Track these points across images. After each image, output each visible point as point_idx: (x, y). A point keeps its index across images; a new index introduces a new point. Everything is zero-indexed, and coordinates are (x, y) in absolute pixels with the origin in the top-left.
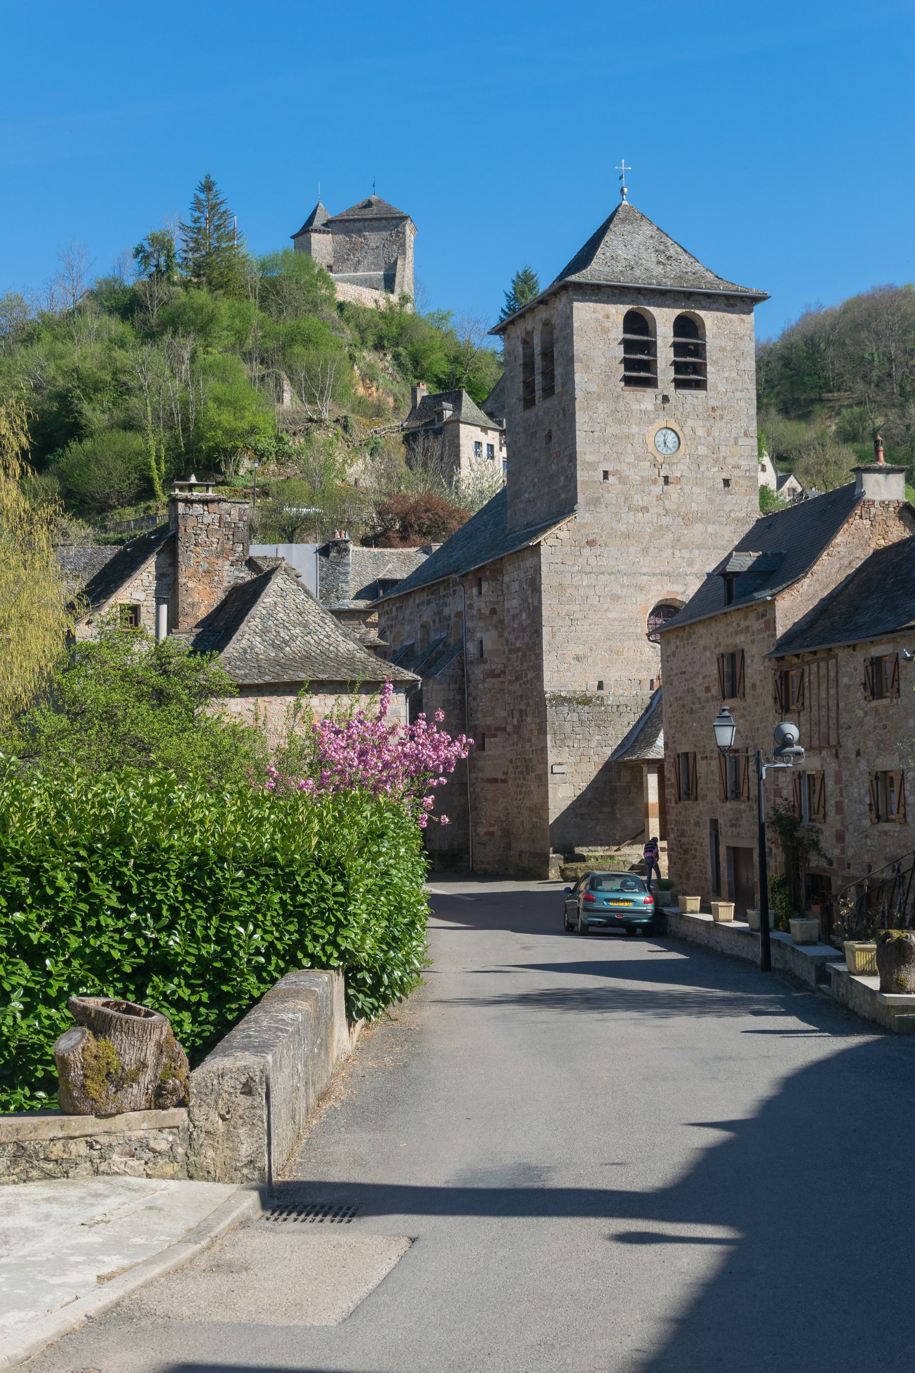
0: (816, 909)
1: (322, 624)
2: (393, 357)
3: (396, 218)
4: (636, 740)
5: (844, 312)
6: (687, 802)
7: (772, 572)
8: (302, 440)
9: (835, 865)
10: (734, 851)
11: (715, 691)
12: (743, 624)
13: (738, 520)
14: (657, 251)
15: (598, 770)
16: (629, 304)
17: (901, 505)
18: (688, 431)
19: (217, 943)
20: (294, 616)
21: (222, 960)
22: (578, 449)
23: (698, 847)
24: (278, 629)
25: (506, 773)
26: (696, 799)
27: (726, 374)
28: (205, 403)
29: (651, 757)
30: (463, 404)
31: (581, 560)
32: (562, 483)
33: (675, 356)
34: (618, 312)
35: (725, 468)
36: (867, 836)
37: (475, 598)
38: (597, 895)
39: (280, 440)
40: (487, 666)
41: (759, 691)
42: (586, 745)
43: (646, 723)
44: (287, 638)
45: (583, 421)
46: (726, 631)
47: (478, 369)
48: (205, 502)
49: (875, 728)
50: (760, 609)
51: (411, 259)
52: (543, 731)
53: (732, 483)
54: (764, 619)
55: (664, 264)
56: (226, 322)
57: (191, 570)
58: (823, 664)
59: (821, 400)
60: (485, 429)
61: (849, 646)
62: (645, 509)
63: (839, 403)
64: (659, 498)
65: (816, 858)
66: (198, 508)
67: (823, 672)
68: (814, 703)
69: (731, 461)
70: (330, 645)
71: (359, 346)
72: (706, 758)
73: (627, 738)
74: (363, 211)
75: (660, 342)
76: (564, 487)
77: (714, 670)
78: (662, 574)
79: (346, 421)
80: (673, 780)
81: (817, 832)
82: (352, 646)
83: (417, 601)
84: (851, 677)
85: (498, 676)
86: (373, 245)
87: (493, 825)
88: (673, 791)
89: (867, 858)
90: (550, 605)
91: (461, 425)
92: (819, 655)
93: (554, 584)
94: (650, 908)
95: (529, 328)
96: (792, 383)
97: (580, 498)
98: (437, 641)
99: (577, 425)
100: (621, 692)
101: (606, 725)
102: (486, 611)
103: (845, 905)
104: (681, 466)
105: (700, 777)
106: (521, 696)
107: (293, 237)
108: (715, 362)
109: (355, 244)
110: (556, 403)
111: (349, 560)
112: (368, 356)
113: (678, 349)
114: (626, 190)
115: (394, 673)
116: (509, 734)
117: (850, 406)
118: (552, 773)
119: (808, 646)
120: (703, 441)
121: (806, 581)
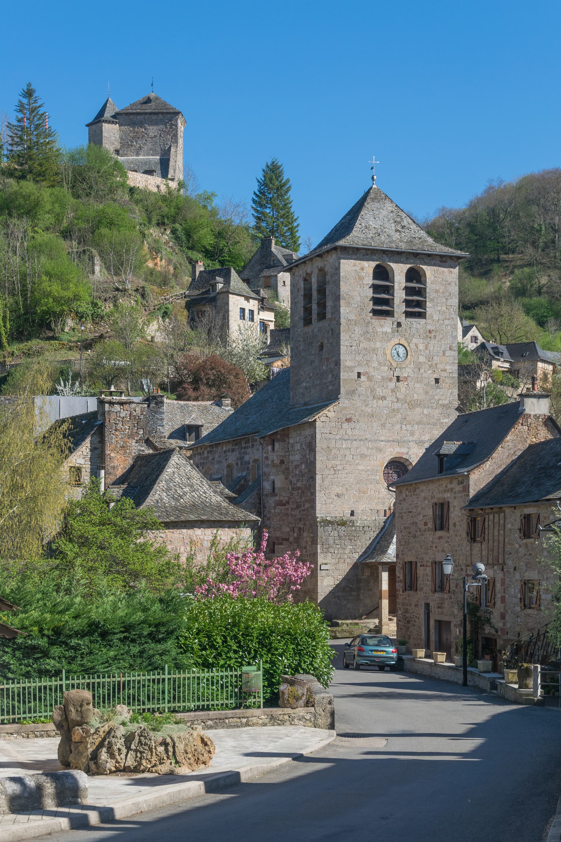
0: (487, 657)
1: (201, 485)
2: (172, 231)
3: (170, 113)
4: (374, 549)
5: (519, 188)
6: (410, 592)
7: (468, 454)
8: (111, 305)
9: (499, 632)
10: (439, 623)
11: (430, 525)
12: (449, 486)
13: (443, 406)
14: (395, 222)
15: (349, 568)
16: (377, 261)
17: (546, 417)
18: (413, 346)
19: (270, 664)
20: (185, 480)
21: (273, 670)
22: (342, 358)
23: (417, 620)
24: (176, 488)
26: (416, 590)
27: (439, 308)
28: (40, 276)
29: (384, 561)
30: (232, 279)
31: (342, 432)
32: (329, 379)
33: (406, 295)
34: (369, 266)
35: (436, 371)
36: (518, 617)
37: (269, 452)
38: (365, 648)
39: (95, 305)
40: (277, 498)
41: (458, 528)
42: (342, 552)
43: (381, 538)
44: (181, 493)
45: (345, 339)
46: (438, 489)
47: (236, 243)
48: (121, 404)
49: (525, 555)
50: (460, 479)
51: (181, 146)
52: (314, 542)
53: (441, 381)
54: (462, 485)
55: (400, 232)
56: (48, 207)
57: (113, 446)
58: (496, 515)
59: (498, 261)
60: (247, 298)
61: (512, 507)
62: (384, 398)
63: (513, 263)
64: (393, 391)
65: (489, 628)
66: (117, 407)
67: (496, 520)
68: (491, 538)
69: (440, 366)
70: (207, 498)
71: (147, 224)
72: (423, 565)
73: (368, 548)
74: (144, 106)
75: (396, 287)
76: (331, 382)
77: (430, 512)
78: (393, 441)
79: (144, 290)
80: (401, 578)
81: (490, 613)
82: (219, 499)
83: (224, 449)
84: (512, 525)
85: (285, 505)
86: (152, 134)
88: (401, 585)
89: (517, 629)
90: (321, 460)
91: (230, 296)
92: (494, 510)
93: (324, 447)
94: (395, 655)
95: (309, 271)
96: (476, 246)
97: (342, 390)
98: (239, 477)
99: (341, 341)
100: (365, 517)
101: (355, 539)
102: (277, 462)
103: (505, 654)
104: (408, 370)
105: (419, 577)
106: (300, 519)
107: (87, 125)
108: (432, 300)
109: (137, 133)
110: (327, 325)
111: (163, 409)
112: (154, 232)
113: (409, 291)
114: (375, 177)
115: (244, 516)
116: (291, 543)
117: (521, 266)
118: (321, 570)
119: (488, 504)
120: (422, 353)
121: (488, 463)
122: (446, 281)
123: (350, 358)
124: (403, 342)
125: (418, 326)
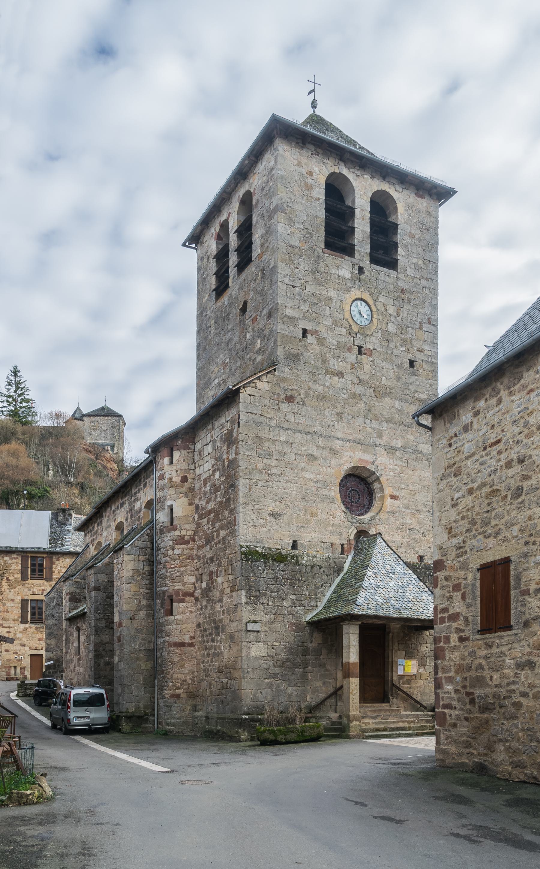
25: (192, 638)
27: (414, 261)
35: (411, 350)
37: (166, 467)
40: (177, 533)
53: (417, 364)
62: (340, 375)
69: (418, 344)
78: (354, 441)
85: (188, 542)
87: (179, 688)
100: (314, 553)
102: (177, 479)
104: (374, 340)
120: (393, 320)
122: (423, 225)
123: (292, 304)
124: (367, 296)
125: (387, 279)
